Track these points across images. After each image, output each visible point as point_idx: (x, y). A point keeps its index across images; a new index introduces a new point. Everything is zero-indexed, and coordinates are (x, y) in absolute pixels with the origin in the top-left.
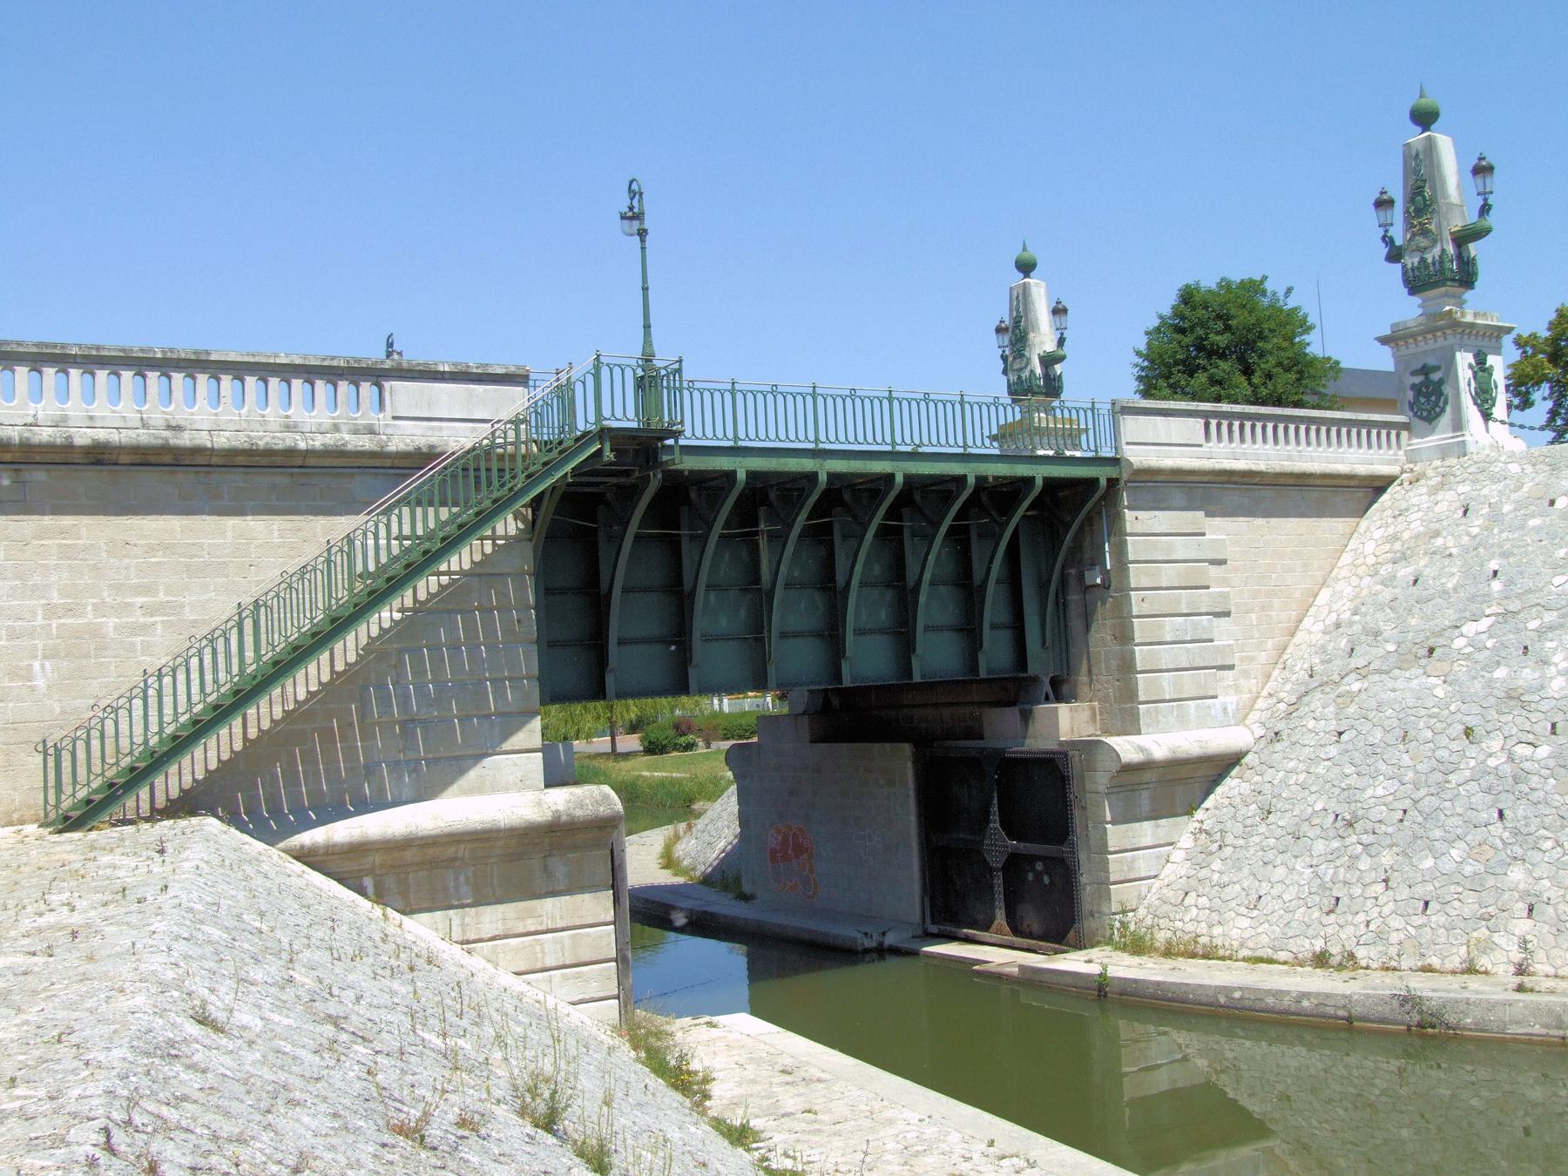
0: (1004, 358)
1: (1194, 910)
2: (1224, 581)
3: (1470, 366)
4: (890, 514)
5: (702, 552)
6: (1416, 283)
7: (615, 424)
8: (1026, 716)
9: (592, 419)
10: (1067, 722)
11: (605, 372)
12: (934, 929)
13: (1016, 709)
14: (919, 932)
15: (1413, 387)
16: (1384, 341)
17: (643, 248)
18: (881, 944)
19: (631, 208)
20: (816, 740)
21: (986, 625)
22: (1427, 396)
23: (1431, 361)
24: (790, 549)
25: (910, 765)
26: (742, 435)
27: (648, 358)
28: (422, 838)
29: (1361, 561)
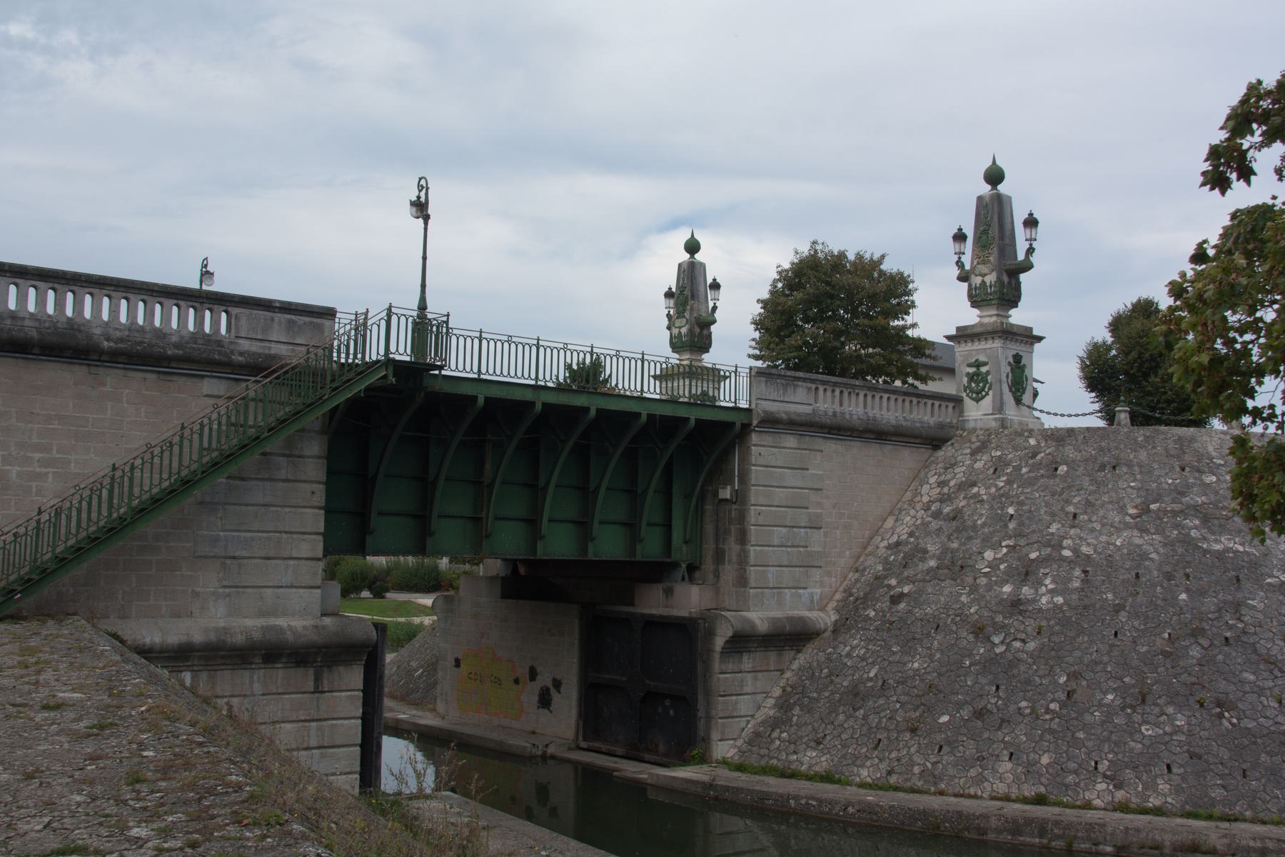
0: (668, 315)
1: (778, 742)
3: (1009, 363)
6: (977, 299)
7: (398, 357)
8: (669, 592)
9: (382, 352)
10: (690, 599)
11: (394, 319)
12: (583, 744)
13: (661, 586)
14: (573, 746)
15: (968, 374)
17: (426, 229)
18: (545, 753)
19: (419, 197)
20: (505, 596)
21: (596, 520)
22: (977, 383)
23: (982, 358)
27: (423, 306)
29: (918, 498)
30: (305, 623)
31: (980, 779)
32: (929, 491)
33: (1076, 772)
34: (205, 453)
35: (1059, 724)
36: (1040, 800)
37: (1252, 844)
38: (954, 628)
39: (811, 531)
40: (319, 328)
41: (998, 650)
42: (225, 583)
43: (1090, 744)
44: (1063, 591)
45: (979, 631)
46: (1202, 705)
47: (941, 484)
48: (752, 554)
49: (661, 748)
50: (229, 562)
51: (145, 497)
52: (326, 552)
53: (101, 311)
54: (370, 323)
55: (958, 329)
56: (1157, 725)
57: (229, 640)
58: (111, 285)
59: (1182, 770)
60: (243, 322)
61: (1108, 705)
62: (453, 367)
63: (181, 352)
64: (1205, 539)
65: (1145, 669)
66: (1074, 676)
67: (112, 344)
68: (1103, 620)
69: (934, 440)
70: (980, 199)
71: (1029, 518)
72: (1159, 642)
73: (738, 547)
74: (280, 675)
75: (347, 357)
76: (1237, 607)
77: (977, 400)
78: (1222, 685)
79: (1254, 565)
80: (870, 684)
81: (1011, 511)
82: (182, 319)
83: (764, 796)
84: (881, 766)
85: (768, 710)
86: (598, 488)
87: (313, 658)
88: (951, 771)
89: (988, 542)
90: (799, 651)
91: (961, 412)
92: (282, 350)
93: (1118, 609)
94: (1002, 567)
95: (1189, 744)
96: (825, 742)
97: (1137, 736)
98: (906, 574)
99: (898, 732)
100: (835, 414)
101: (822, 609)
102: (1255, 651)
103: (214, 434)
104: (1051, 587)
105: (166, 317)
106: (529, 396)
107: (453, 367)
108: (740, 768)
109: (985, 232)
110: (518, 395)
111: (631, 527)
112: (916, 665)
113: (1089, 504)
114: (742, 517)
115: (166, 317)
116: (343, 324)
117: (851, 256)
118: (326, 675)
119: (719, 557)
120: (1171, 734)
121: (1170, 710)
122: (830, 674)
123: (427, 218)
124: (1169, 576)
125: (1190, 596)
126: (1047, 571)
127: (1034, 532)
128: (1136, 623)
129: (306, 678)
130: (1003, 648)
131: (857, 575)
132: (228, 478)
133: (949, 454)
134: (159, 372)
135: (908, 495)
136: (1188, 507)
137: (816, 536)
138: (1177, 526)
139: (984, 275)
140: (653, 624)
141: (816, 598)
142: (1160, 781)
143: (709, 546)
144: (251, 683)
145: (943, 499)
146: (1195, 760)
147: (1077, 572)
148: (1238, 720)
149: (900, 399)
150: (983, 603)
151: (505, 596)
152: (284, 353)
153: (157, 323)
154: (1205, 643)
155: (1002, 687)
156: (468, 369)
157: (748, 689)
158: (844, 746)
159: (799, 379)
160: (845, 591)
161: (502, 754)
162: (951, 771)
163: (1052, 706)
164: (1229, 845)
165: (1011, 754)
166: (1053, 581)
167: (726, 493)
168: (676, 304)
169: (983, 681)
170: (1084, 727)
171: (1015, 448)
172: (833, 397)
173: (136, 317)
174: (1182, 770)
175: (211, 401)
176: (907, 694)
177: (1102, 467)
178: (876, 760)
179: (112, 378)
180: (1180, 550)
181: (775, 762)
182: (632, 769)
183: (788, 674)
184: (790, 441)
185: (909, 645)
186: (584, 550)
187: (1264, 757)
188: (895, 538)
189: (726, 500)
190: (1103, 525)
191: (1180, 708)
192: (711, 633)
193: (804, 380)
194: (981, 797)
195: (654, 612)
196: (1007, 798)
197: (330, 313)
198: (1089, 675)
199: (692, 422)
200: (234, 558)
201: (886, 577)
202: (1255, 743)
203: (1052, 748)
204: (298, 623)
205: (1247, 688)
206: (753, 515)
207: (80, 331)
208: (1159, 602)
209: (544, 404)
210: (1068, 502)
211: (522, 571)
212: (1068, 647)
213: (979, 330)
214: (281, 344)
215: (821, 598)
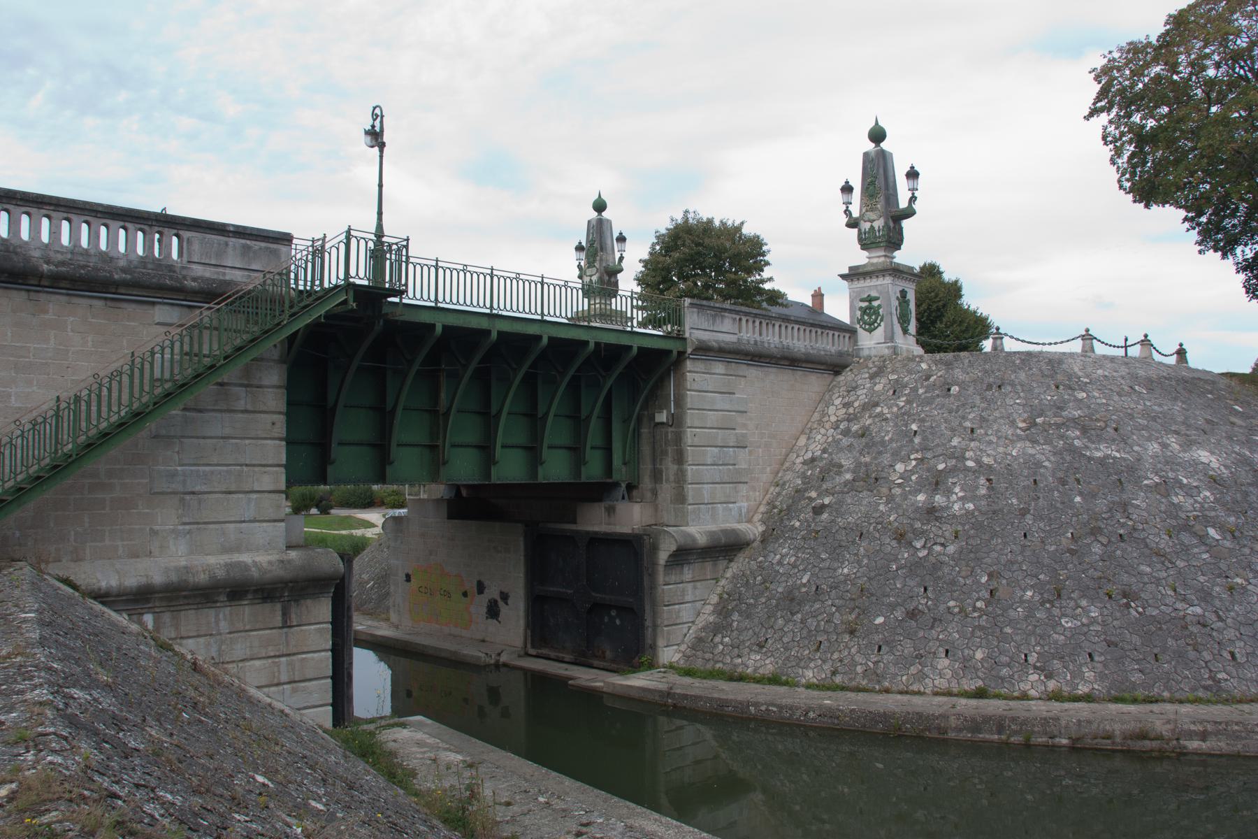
0: (579, 266)
1: (721, 647)
2: (744, 426)
4: (533, 366)
5: (343, 381)
6: (866, 243)
7: (358, 282)
8: (611, 510)
9: (342, 276)
11: (354, 242)
12: (532, 652)
13: (603, 505)
15: (861, 308)
16: (843, 277)
17: (381, 157)
19: (373, 126)
20: (451, 516)
23: (874, 294)
27: (379, 233)
29: (826, 419)
30: (270, 558)
31: (921, 676)
32: (835, 411)
33: (1008, 665)
34: (158, 384)
35: (987, 621)
36: (980, 694)
37: (1193, 727)
38: (877, 535)
39: (735, 453)
40: (276, 253)
41: (921, 555)
42: (186, 520)
43: (1018, 638)
44: (973, 499)
45: (900, 537)
46: (1110, 597)
47: (847, 405)
48: (689, 473)
49: (608, 654)
50: (188, 497)
51: (93, 432)
52: (290, 483)
53: (39, 232)
54: (327, 246)
55: (850, 268)
56: (1074, 617)
57: (191, 580)
58: (50, 204)
59: (1103, 658)
60: (196, 246)
61: (1029, 601)
62: (411, 295)
63: (129, 277)
64: (1087, 447)
65: (1057, 567)
67: (52, 267)
68: (1013, 524)
69: (835, 367)
70: (866, 155)
71: (932, 433)
72: (1064, 541)
73: (676, 467)
74: (247, 611)
75: (305, 285)
76: (1125, 506)
77: (870, 331)
78: (1125, 577)
79: (1131, 469)
80: (804, 590)
81: (914, 427)
82: (130, 243)
83: (723, 703)
84: (825, 667)
85: (708, 616)
86: (547, 414)
87: (278, 593)
88: (892, 669)
89: (898, 456)
90: (731, 561)
91: (856, 342)
92: (238, 276)
93: (1024, 512)
94: (913, 478)
95: (1105, 633)
96: (768, 645)
98: (824, 486)
99: (838, 634)
100: (756, 342)
101: (749, 521)
102: (1147, 546)
103: (167, 364)
104: (961, 494)
105: (113, 241)
106: (484, 324)
107: (411, 295)
108: (688, 673)
109: (872, 183)
110: (474, 323)
111: (576, 451)
112: (846, 571)
113: (983, 420)
114: (679, 439)
115: (113, 241)
116: (300, 248)
117: (717, 223)
118: (294, 610)
119: (657, 476)
120: (1088, 625)
121: (1084, 603)
122: (764, 582)
123: (382, 146)
124: (1063, 482)
125: (1083, 499)
126: (955, 480)
127: (938, 445)
128: (1042, 525)
129: (273, 613)
130: (926, 552)
131: (778, 489)
132: (185, 409)
133: (849, 379)
134: (106, 299)
135: (816, 416)
136: (1068, 420)
137: (742, 455)
138: (1062, 437)
139: (872, 221)
140: (598, 541)
141: (744, 511)
142: (1085, 669)
143: (646, 468)
144: (217, 622)
145: (850, 419)
146: (1112, 648)
147: (982, 481)
148: (1144, 608)
149: (808, 329)
150: (901, 512)
151: (451, 516)
152: (239, 279)
153: (103, 247)
154: (1105, 541)
155: (930, 589)
156: (425, 297)
157: (689, 598)
158: (786, 649)
159: (725, 310)
160: (768, 504)
161: (456, 663)
162: (892, 669)
163: (979, 604)
164: (1173, 731)
165: (947, 651)
166: (962, 489)
167: (662, 417)
168: (587, 257)
169: (912, 583)
170: (1011, 622)
171: (910, 372)
172: (754, 327)
173: (79, 239)
174: (1103, 658)
175: (163, 329)
176: (842, 598)
177: (989, 387)
178: (820, 662)
179: (54, 305)
180: (1068, 458)
181: (719, 665)
182: (586, 677)
183: (723, 582)
184: (719, 368)
185: (837, 552)
186: (534, 474)
187: (1170, 642)
188: (809, 455)
189: (662, 423)
190: (999, 438)
191: (1092, 600)
192: (655, 548)
193: (730, 311)
194: (924, 693)
195: (596, 529)
196: (949, 694)
197: (286, 239)
198: (1007, 574)
199: (635, 350)
200: (193, 493)
201: (806, 490)
202: (1160, 629)
203: (984, 644)
204: (263, 559)
205: (1146, 580)
206: (690, 436)
207: (16, 253)
208: (1058, 505)
209: (499, 332)
210: (964, 418)
211: (464, 493)
212: (985, 549)
213: (870, 269)
214: (236, 270)
215: (748, 512)
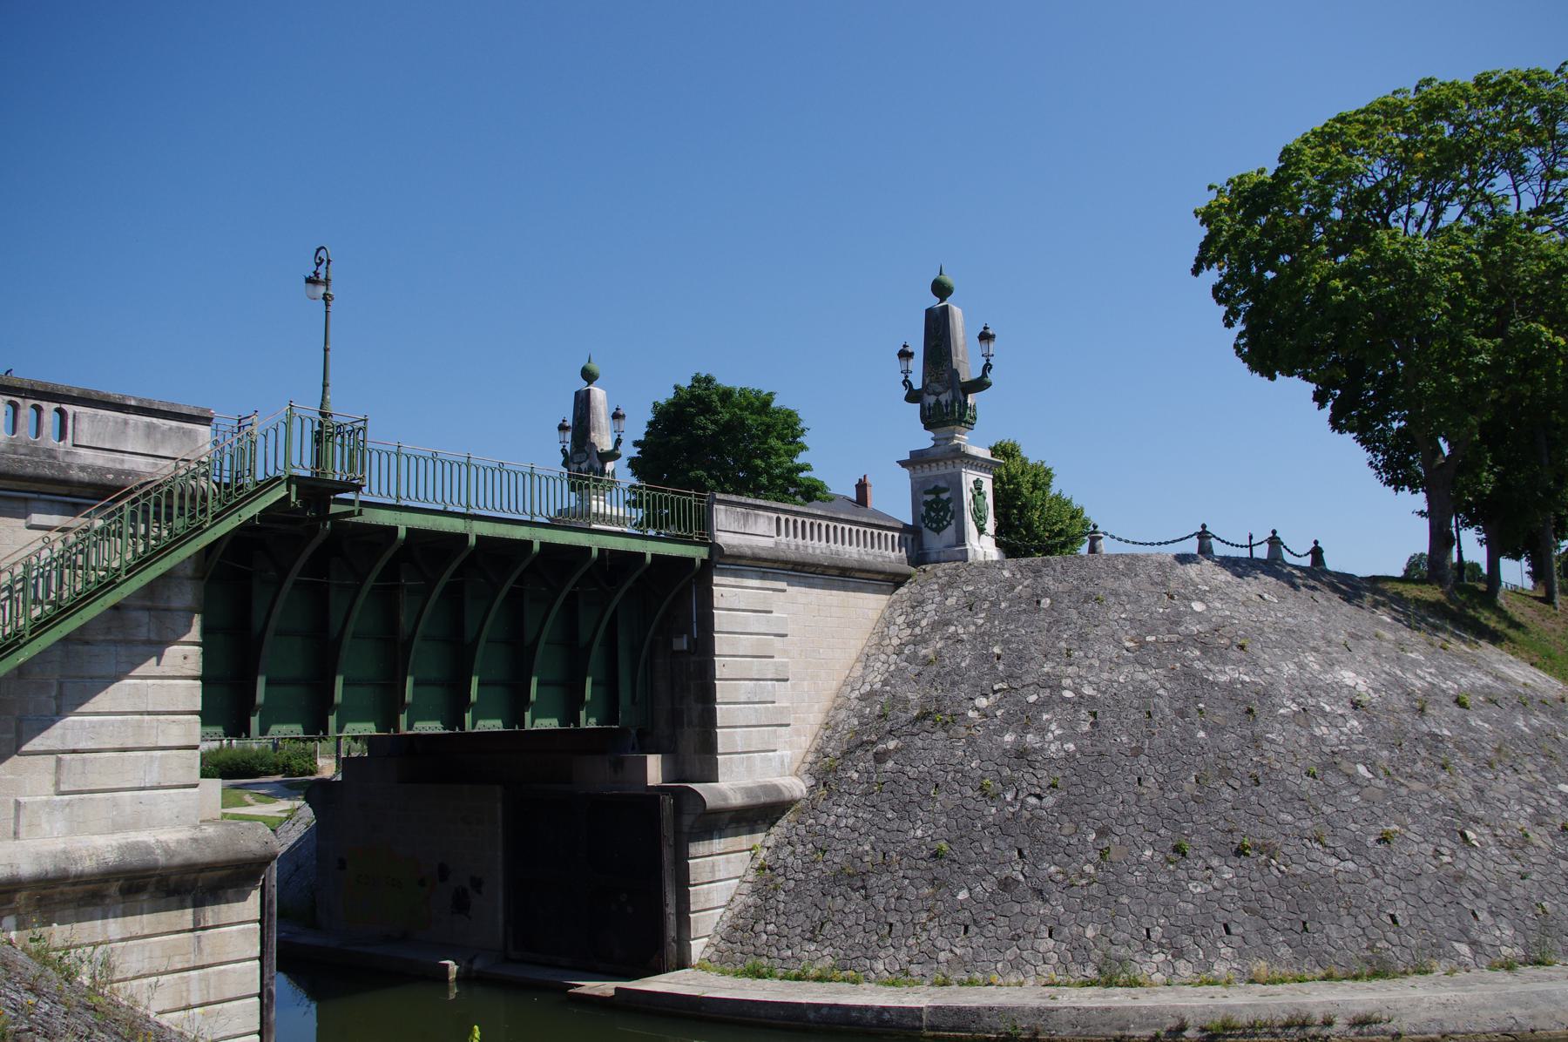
0: (563, 451)
1: (764, 937)
2: (785, 652)
4: (519, 580)
9: (281, 465)
11: (296, 423)
15: (926, 503)
16: (903, 464)
19: (316, 274)
22: (937, 511)
23: (942, 484)
24: (360, 601)
25: (499, 805)
26: (404, 494)
28: (129, 871)
66: (1102, 833)
73: (700, 706)
76: (1256, 741)
77: (938, 530)
81: (997, 650)
90: (773, 824)
92: (141, 464)
97: (1186, 895)
104: (1057, 732)
112: (919, 833)
124: (1182, 713)
125: (1208, 734)
139: (938, 394)
141: (787, 760)
145: (917, 641)
147: (1083, 714)
152: (142, 468)
166: (1060, 726)
167: (682, 644)
185: (905, 811)
189: (682, 652)
190: (1102, 661)
209: (478, 537)
